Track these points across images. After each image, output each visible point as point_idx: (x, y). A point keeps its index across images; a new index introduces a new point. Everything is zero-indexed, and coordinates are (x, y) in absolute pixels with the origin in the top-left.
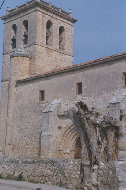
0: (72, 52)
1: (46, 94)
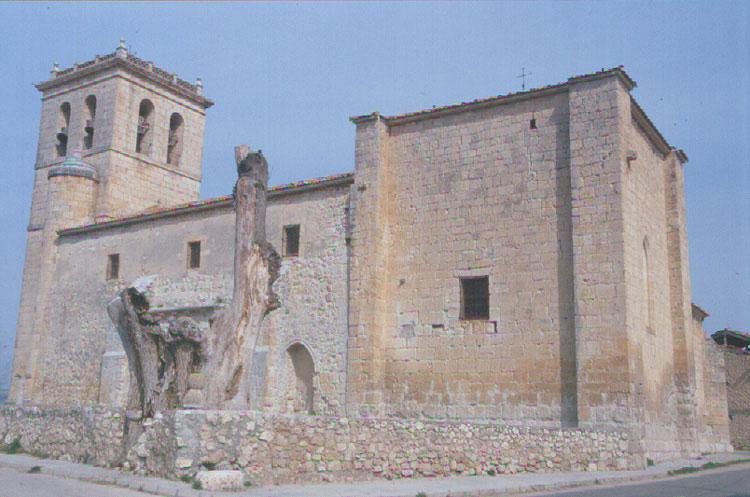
0: (198, 172)
1: (123, 262)
